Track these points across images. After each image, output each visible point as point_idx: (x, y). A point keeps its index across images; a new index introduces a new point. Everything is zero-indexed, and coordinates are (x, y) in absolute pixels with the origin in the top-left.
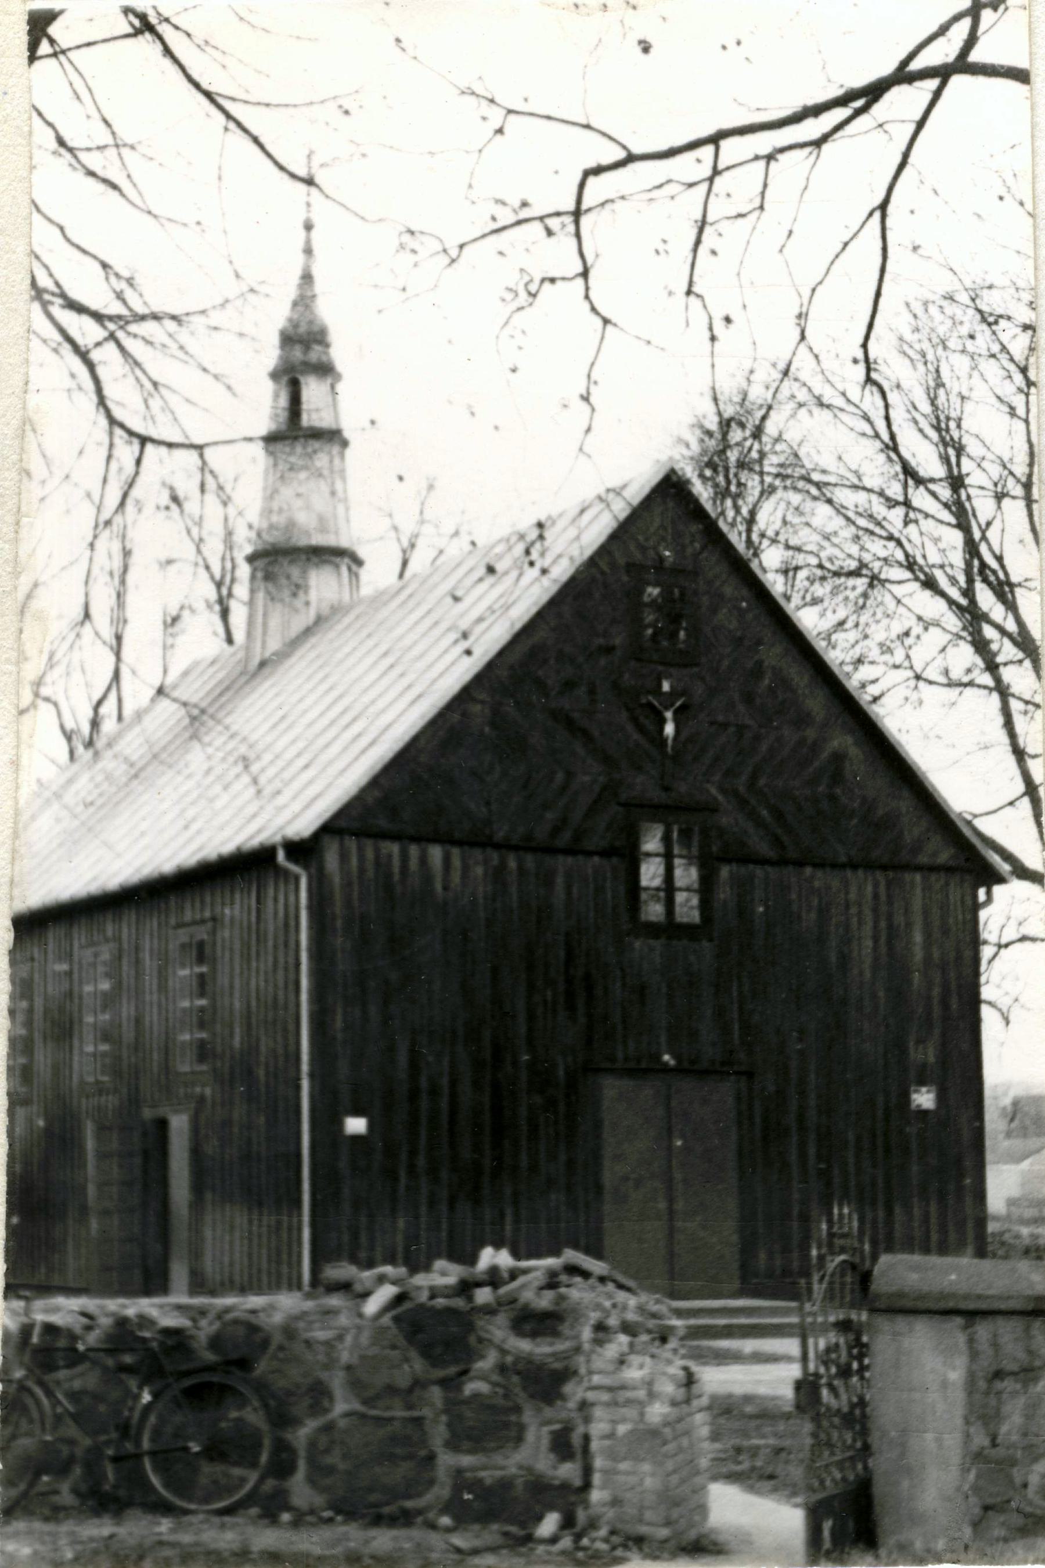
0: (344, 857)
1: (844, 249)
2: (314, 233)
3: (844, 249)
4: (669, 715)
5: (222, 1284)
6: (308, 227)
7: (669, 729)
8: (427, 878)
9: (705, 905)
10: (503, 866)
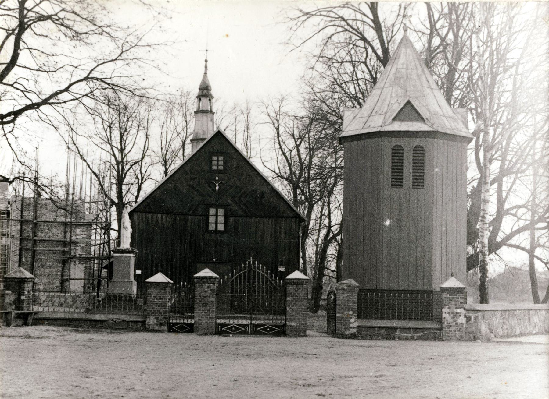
0: (139, 217)
1: (9, 143)
2: (208, 63)
3: (9, 143)
4: (217, 185)
5: (120, 300)
6: (206, 61)
7: (217, 188)
8: (157, 221)
9: (225, 226)
10: (175, 219)
